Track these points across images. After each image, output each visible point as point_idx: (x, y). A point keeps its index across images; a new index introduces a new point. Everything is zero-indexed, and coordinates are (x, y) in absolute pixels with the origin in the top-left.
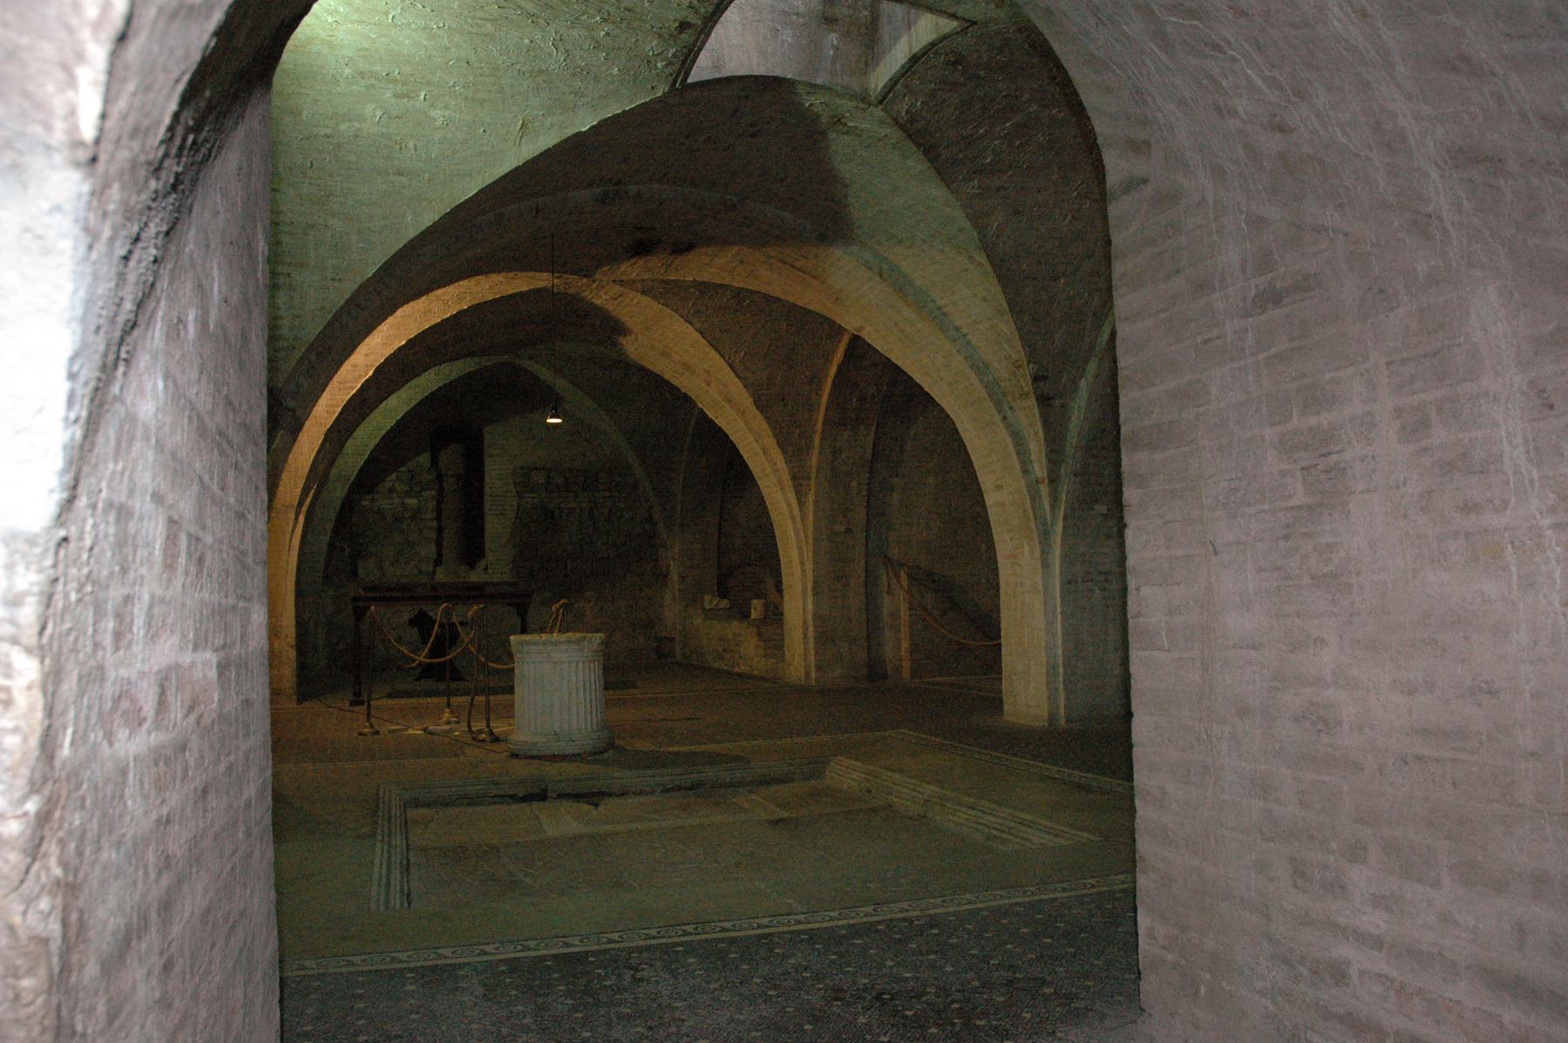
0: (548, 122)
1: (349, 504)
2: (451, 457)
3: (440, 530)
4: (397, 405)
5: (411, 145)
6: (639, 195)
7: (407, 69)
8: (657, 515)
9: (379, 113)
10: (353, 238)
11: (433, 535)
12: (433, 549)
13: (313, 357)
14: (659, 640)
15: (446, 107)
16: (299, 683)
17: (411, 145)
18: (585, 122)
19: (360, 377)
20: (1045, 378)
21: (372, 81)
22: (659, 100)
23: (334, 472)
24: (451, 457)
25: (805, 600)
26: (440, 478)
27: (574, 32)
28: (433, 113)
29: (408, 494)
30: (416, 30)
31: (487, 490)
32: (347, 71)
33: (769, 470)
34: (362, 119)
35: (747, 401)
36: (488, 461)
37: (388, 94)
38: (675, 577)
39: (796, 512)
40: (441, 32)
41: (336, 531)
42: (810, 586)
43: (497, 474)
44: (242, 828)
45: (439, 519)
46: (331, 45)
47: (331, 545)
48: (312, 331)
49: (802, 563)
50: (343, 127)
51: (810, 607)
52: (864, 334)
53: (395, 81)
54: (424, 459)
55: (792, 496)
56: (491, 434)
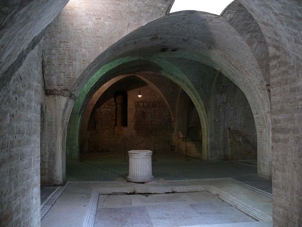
0: (135, 24)
1: (94, 110)
2: (119, 98)
3: (116, 117)
4: (106, 86)
5: (100, 30)
6: (161, 38)
7: (98, 13)
8: (171, 114)
9: (92, 23)
10: (87, 53)
11: (115, 118)
12: (114, 122)
13: (79, 81)
14: (171, 146)
15: (109, 21)
16: (66, 174)
17: (100, 30)
18: (144, 23)
19: (95, 81)
20: (269, 85)
21: (90, 16)
22: (163, 17)
23: (90, 102)
24: (119, 98)
25: (207, 139)
26: (116, 104)
27: (139, 2)
28: (106, 23)
29: (108, 108)
30: (100, 3)
31: (128, 107)
32: (84, 14)
33: (199, 105)
34: (88, 25)
35: (193, 87)
36: (128, 100)
37: (94, 19)
38: (176, 130)
39: (206, 116)
40: (106, 4)
41: (90, 117)
42: (209, 135)
43: (130, 103)
44: (178, 74)
45: (116, 114)
46: (79, 8)
47: (89, 121)
48: (78, 76)
49: (207, 129)
50: (84, 27)
51: (209, 140)
52: (222, 72)
53: (96, 16)
54: (113, 99)
55: (205, 112)
56: (130, 93)
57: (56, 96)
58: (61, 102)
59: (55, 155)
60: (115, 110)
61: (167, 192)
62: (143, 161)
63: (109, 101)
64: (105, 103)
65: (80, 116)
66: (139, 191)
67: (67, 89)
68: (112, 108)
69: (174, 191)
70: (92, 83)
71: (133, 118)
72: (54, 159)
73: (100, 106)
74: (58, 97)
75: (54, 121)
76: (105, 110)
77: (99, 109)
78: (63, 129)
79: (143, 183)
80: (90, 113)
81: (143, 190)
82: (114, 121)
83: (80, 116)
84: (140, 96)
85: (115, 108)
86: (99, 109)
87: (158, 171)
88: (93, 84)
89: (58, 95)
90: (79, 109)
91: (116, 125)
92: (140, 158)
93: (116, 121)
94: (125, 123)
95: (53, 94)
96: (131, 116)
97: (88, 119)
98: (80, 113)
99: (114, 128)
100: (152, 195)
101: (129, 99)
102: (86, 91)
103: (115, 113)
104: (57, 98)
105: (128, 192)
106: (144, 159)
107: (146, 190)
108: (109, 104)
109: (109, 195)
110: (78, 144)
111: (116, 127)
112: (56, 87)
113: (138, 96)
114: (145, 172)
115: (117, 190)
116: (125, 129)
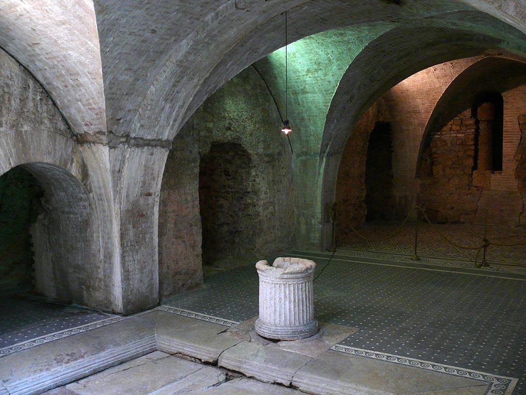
11: (472, 153)
19: (334, 87)
24: (484, 111)
29: (458, 132)
45: (476, 145)
54: (468, 113)
56: (507, 96)
57: (92, 144)
58: (104, 156)
59: (111, 256)
60: (473, 136)
61: (279, 381)
62: (273, 290)
63: (461, 117)
64: (452, 121)
65: (324, 159)
66: (226, 361)
67: (101, 131)
68: (468, 131)
69: (294, 384)
70: (330, 91)
71: (514, 152)
72: (110, 263)
73: (442, 127)
74: (96, 147)
75: (103, 191)
76: (452, 135)
77: (439, 133)
78: (120, 208)
79: (276, 341)
80: (418, 143)
81: (232, 363)
82: (471, 159)
83: (324, 159)
84: (286, 131)
85: (472, 130)
86: (439, 133)
87: (323, 316)
88: (333, 93)
89: (93, 143)
90: (320, 146)
91: (475, 168)
92: (265, 280)
93: (476, 158)
94: (496, 164)
95: (87, 142)
96: (509, 148)
97: (416, 155)
98: (323, 152)
99: (472, 174)
100: (244, 380)
101: (507, 109)
102: (324, 107)
103: (472, 143)
104: (94, 148)
105: (205, 358)
106: (278, 286)
107: (237, 364)
108: (462, 123)
109: (172, 355)
110: (320, 214)
111: (474, 172)
112: (85, 129)
113: (283, 130)
114: (280, 315)
115: (187, 350)
116: (495, 177)
